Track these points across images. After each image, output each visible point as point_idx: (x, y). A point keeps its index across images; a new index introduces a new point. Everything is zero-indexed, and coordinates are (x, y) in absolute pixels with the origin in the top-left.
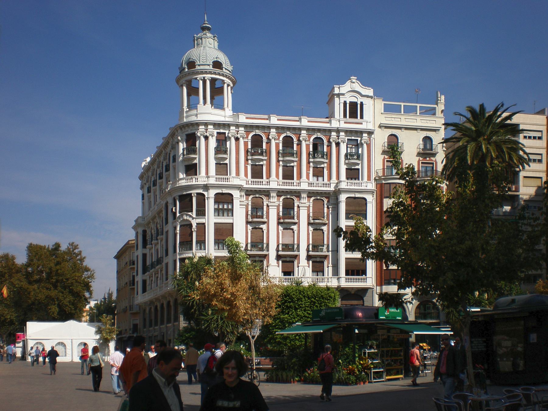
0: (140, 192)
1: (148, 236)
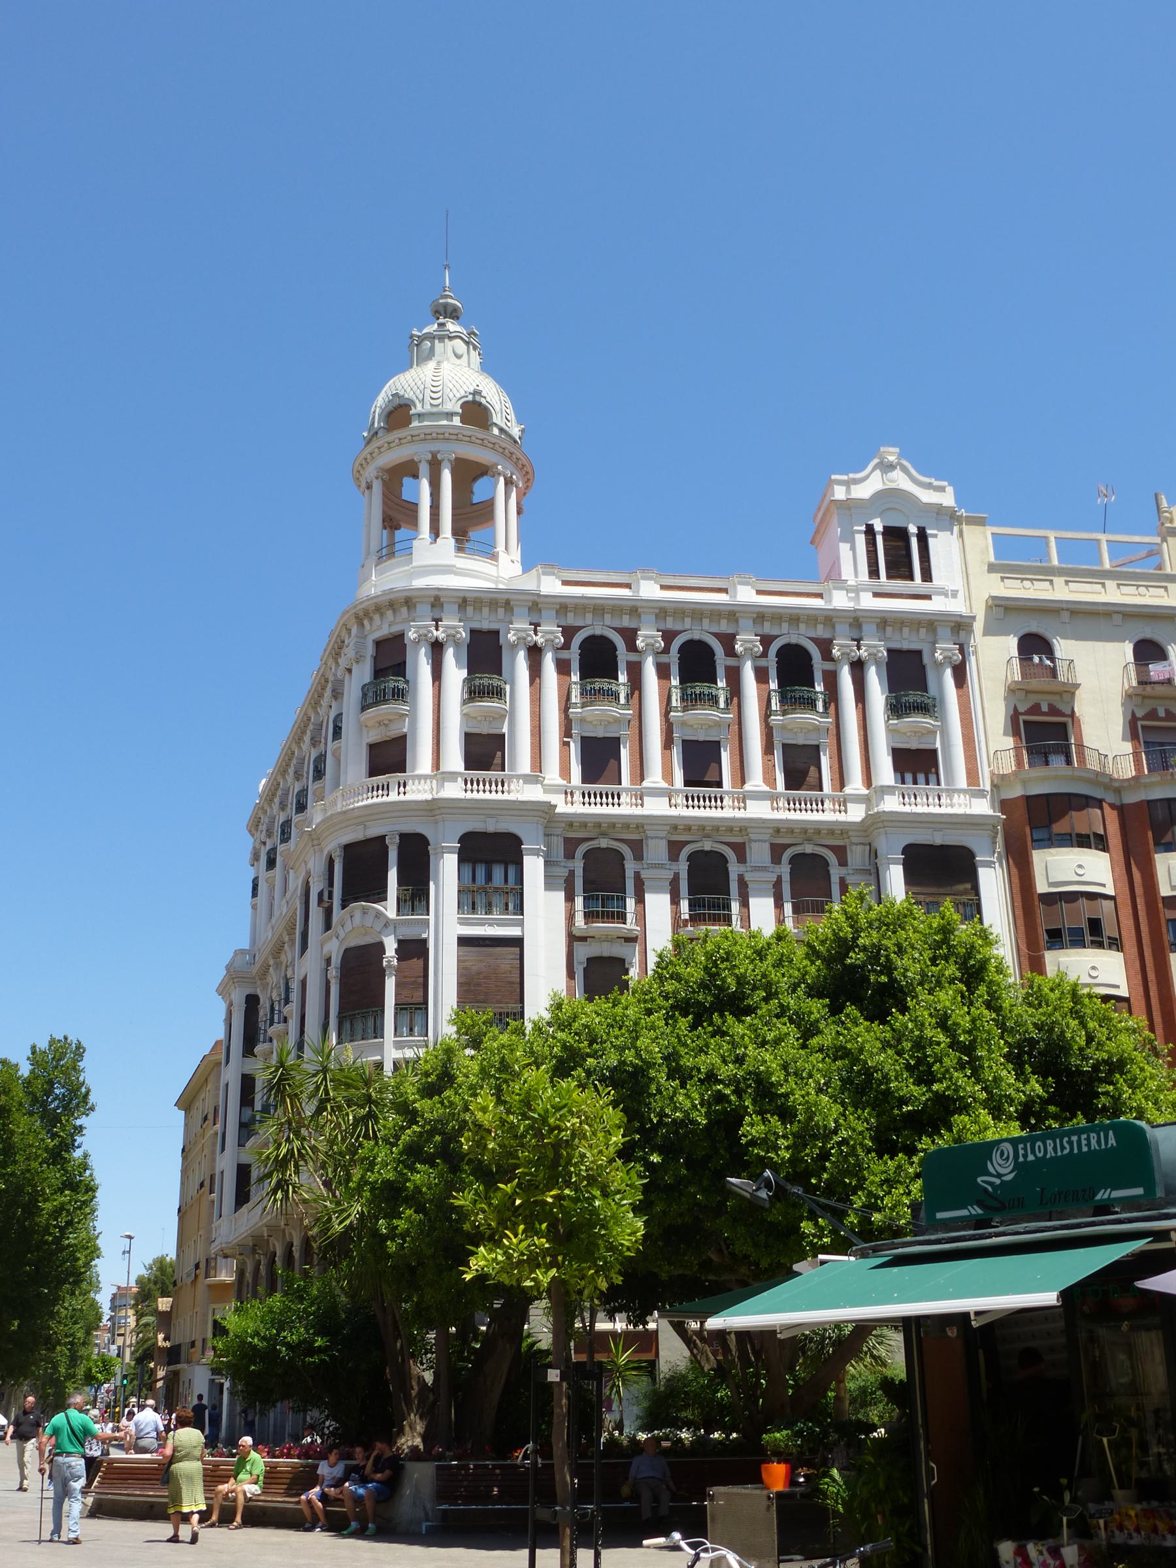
1: (261, 1013)
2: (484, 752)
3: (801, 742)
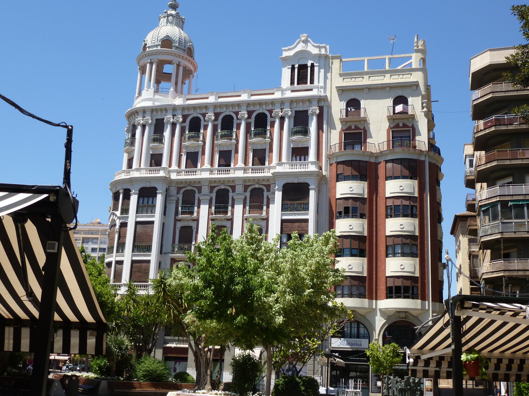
2: (156, 160)
3: (259, 148)
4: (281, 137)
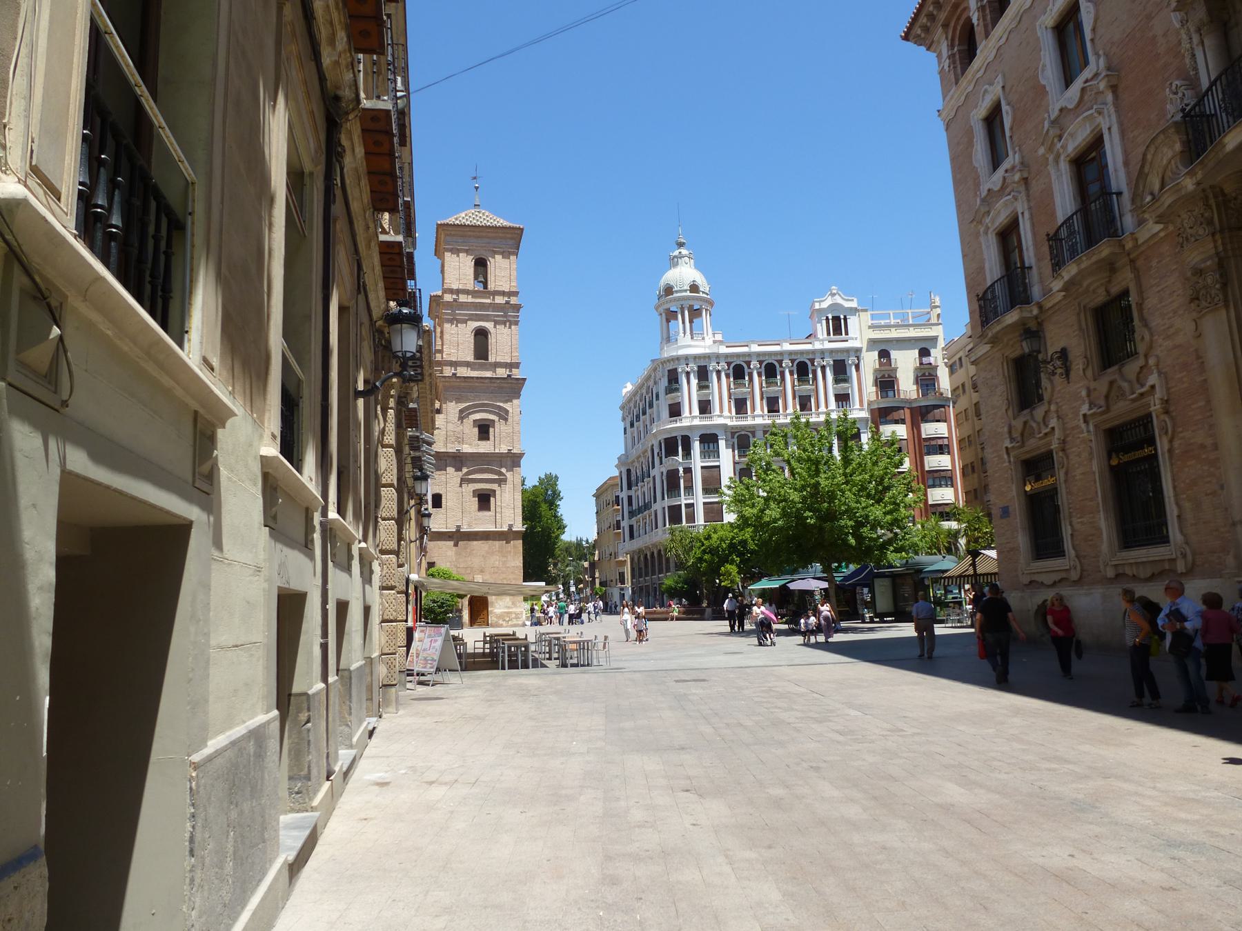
0: (622, 425)
2: (705, 407)
4: (826, 385)
